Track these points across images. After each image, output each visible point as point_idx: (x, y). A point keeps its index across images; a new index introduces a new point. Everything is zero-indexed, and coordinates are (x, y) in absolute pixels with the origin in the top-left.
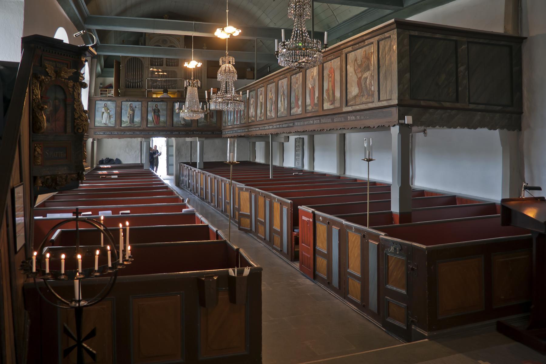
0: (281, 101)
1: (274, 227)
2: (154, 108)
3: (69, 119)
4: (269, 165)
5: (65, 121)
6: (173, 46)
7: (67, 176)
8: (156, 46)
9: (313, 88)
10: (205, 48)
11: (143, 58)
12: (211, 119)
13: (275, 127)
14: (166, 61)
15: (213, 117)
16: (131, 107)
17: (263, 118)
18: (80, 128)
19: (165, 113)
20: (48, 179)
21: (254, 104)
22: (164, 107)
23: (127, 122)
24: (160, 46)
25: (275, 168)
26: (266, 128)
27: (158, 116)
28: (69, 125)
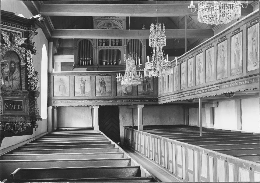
0: (209, 68)
1: (189, 168)
2: (101, 81)
3: (23, 79)
4: (199, 127)
5: (21, 81)
6: (117, 29)
7: (23, 124)
8: (102, 29)
9: (238, 53)
10: (144, 28)
11: (92, 39)
12: (149, 89)
13: (203, 91)
14: (111, 41)
15: (150, 87)
16: (82, 80)
17: (192, 85)
18: (33, 87)
19: (110, 84)
20: (8, 125)
21: (185, 73)
22: (109, 80)
23: (79, 93)
24: (105, 29)
25: (204, 129)
26: (195, 93)
27: (105, 87)
28: (23, 83)
